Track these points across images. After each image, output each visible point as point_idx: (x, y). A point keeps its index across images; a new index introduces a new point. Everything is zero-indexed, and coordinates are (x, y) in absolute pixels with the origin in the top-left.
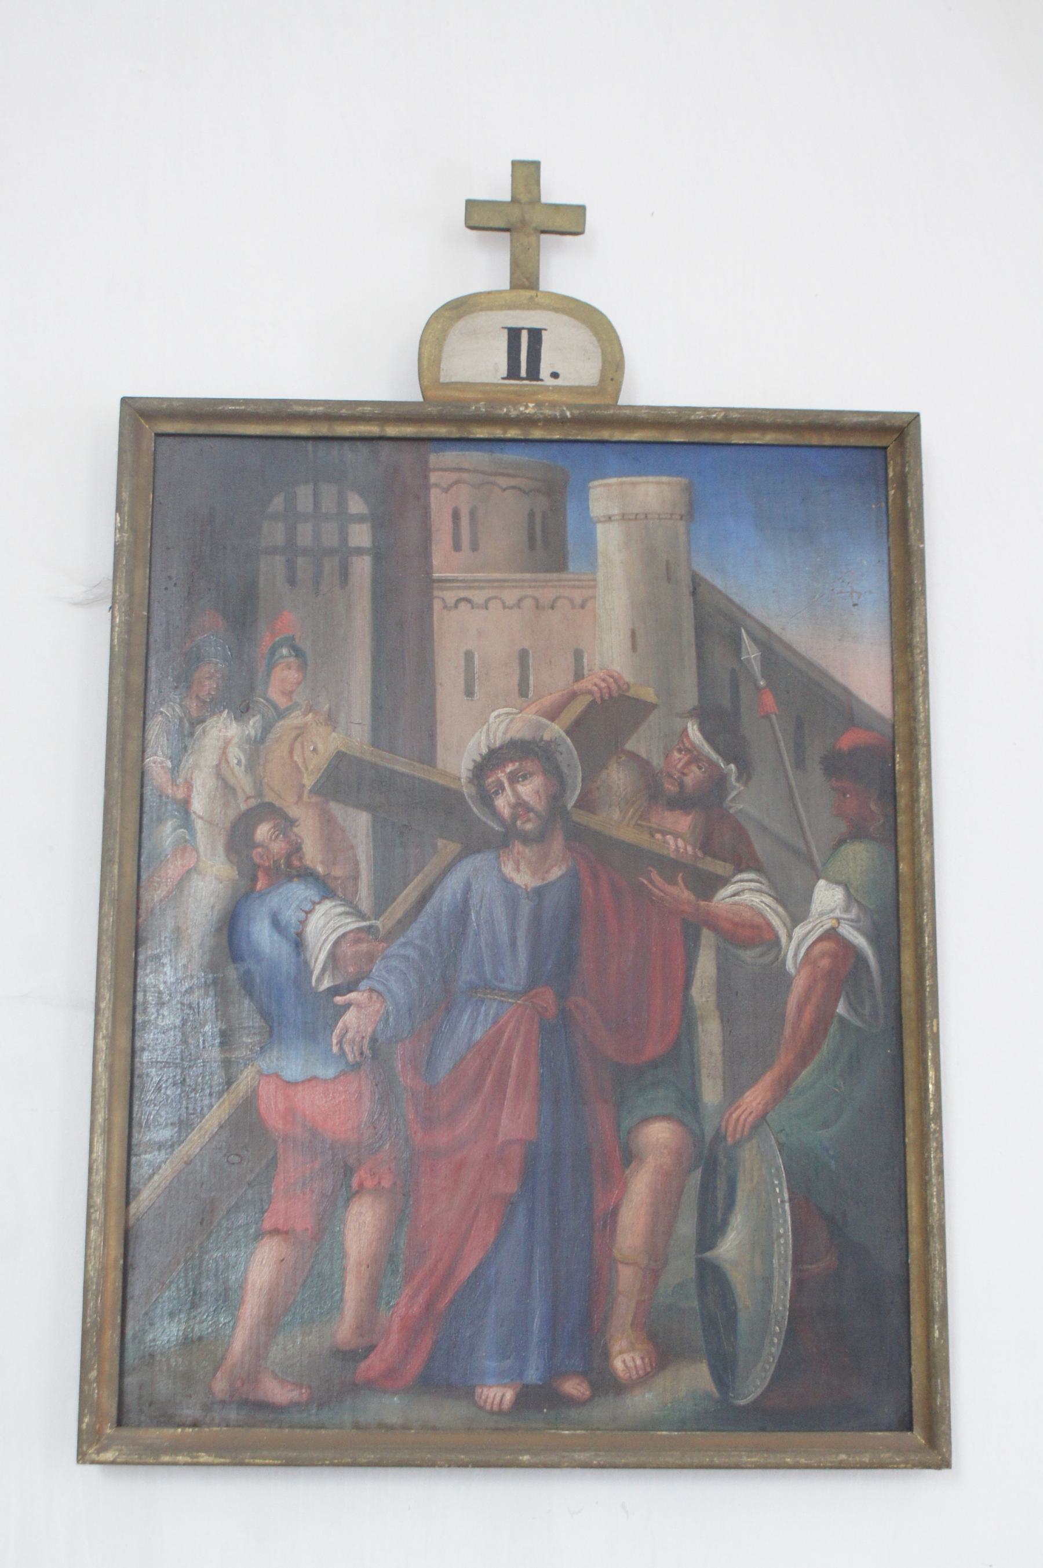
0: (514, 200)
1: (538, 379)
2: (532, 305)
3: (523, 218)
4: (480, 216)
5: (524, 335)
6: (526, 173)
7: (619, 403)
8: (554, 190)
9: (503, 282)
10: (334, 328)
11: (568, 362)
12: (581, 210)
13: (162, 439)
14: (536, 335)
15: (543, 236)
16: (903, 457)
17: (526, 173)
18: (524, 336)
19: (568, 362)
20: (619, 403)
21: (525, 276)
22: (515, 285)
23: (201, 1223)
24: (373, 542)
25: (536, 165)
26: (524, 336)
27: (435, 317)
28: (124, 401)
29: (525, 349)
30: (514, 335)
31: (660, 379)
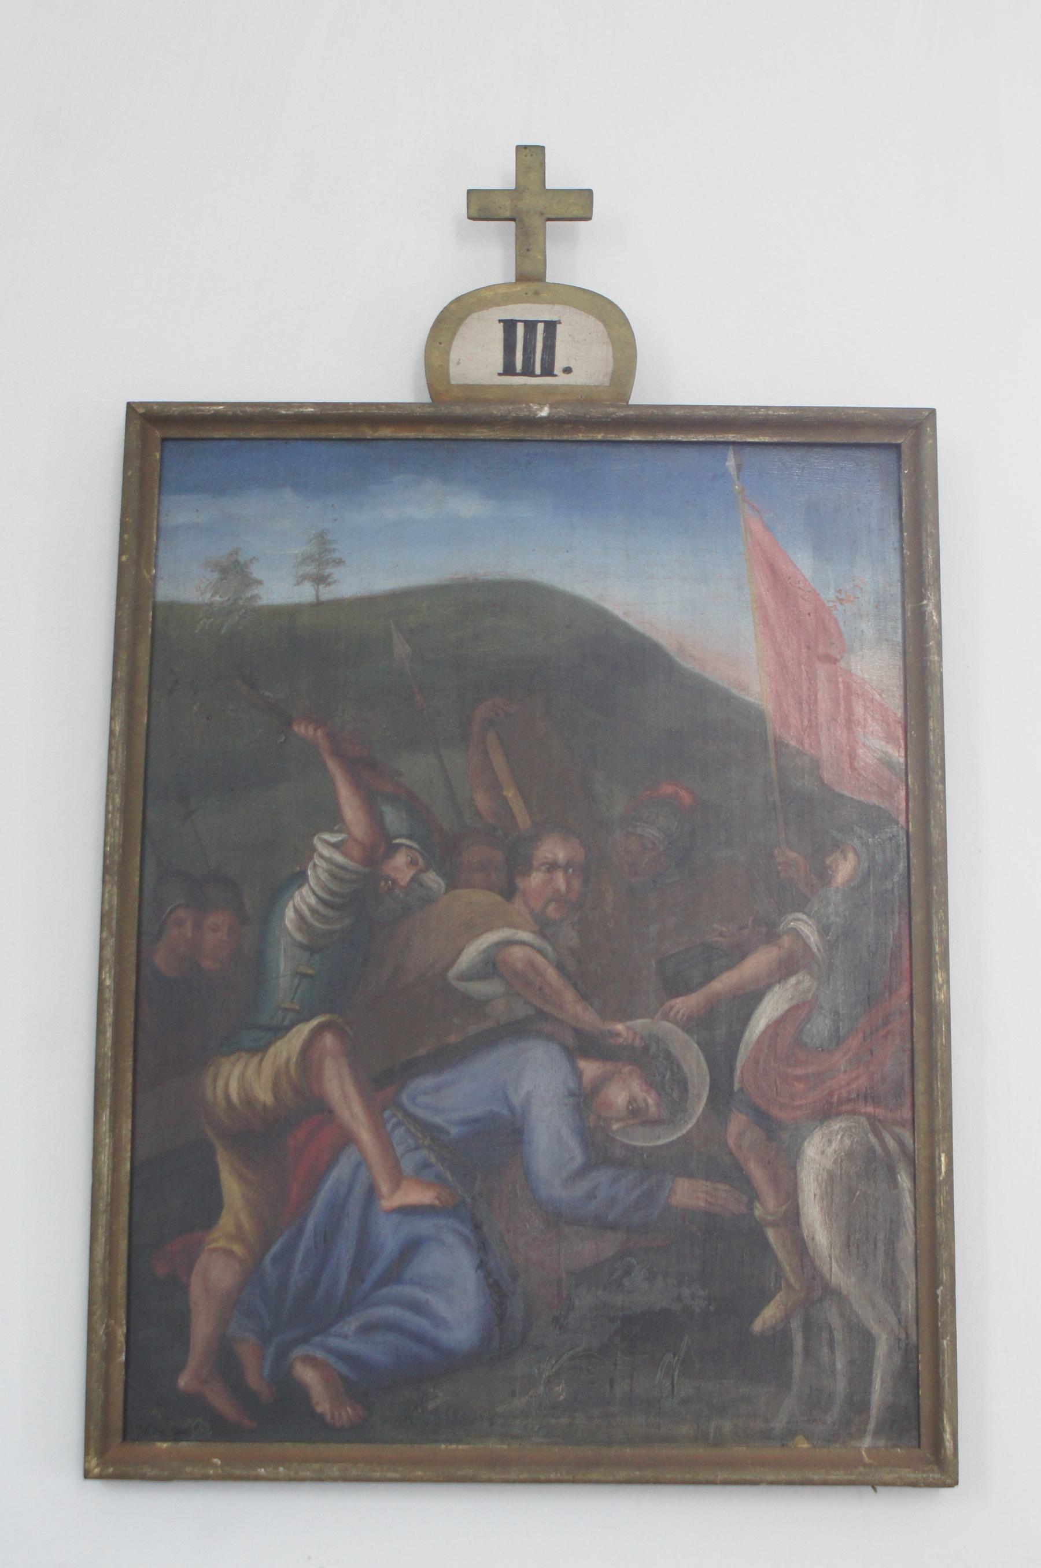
1: (553, 375)
2: (536, 297)
3: (528, 206)
4: (482, 206)
5: (541, 327)
6: (530, 158)
7: (630, 403)
11: (581, 360)
12: (587, 195)
13: (171, 445)
14: (551, 327)
15: (548, 223)
16: (488, 1274)
17: (530, 158)
18: (520, 329)
19: (581, 360)
20: (630, 403)
21: (530, 276)
22: (522, 277)
23: (877, 607)
25: (472, 194)
26: (520, 329)
27: (624, 322)
28: (932, 412)
29: (529, 346)
30: (509, 326)
31: (677, 375)
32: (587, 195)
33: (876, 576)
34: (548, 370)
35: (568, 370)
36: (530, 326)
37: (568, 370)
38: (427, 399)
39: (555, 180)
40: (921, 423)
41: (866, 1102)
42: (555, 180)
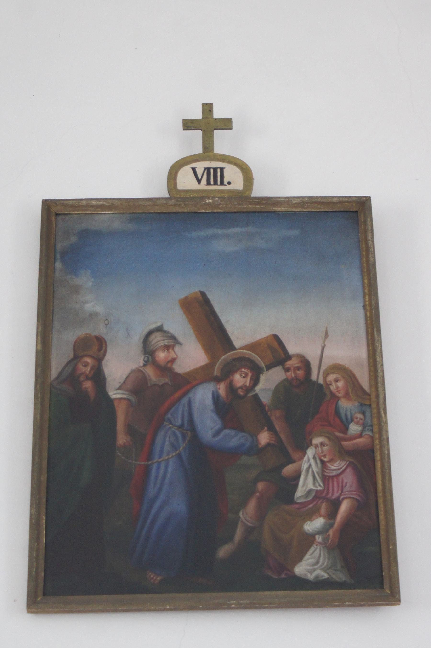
0: (203, 118)
3: (207, 124)
6: (208, 108)
8: (218, 113)
9: (199, 149)
10: (130, 166)
12: (204, 105)
14: (222, 169)
17: (208, 108)
19: (234, 179)
24: (243, 188)
32: (204, 105)
33: (356, 313)
34: (222, 183)
35: (229, 183)
36: (215, 170)
37: (229, 183)
38: (167, 195)
39: (197, 115)
40: (364, 203)
41: (346, 409)
42: (197, 115)
